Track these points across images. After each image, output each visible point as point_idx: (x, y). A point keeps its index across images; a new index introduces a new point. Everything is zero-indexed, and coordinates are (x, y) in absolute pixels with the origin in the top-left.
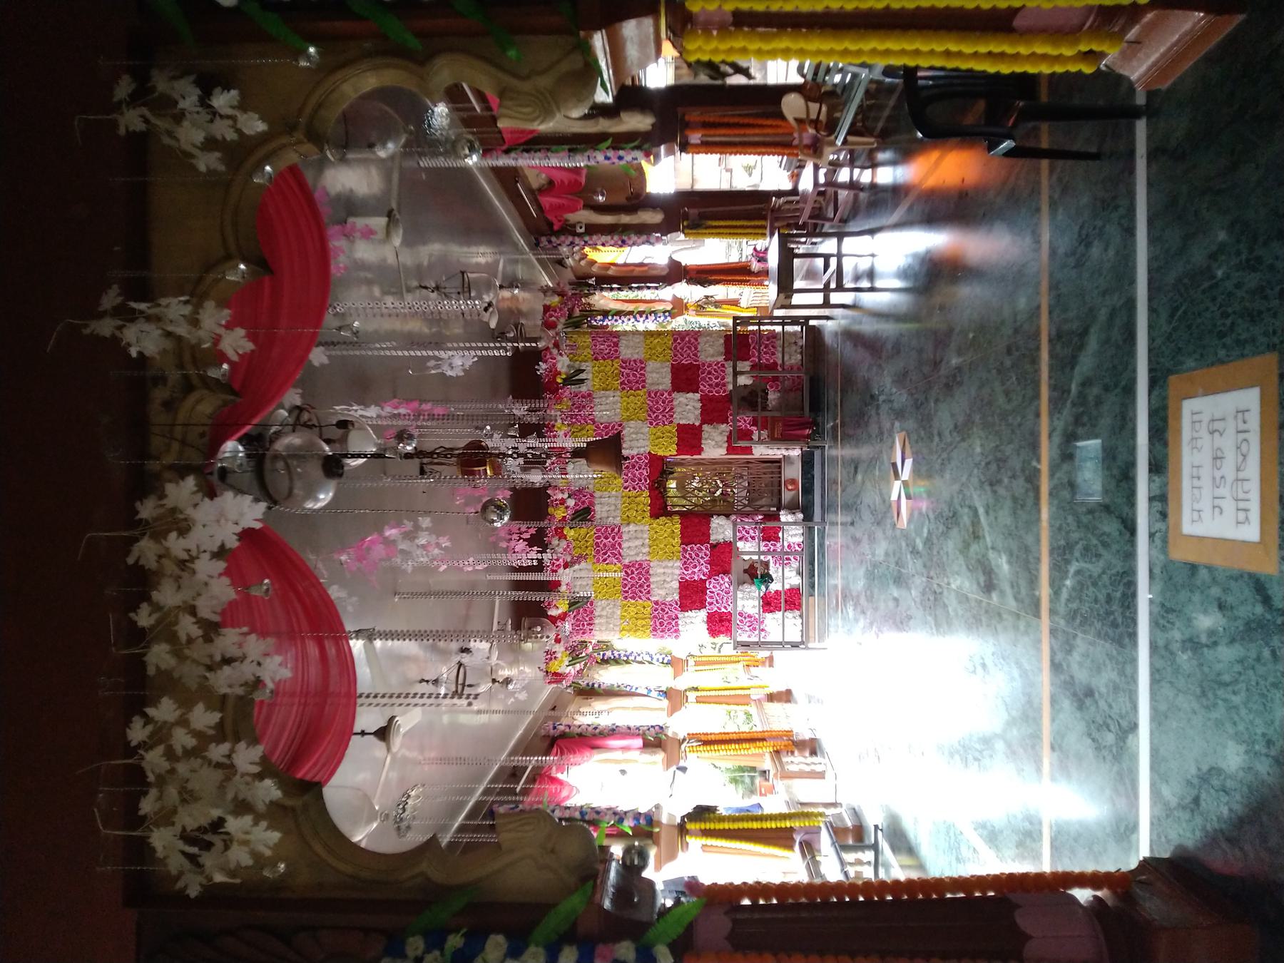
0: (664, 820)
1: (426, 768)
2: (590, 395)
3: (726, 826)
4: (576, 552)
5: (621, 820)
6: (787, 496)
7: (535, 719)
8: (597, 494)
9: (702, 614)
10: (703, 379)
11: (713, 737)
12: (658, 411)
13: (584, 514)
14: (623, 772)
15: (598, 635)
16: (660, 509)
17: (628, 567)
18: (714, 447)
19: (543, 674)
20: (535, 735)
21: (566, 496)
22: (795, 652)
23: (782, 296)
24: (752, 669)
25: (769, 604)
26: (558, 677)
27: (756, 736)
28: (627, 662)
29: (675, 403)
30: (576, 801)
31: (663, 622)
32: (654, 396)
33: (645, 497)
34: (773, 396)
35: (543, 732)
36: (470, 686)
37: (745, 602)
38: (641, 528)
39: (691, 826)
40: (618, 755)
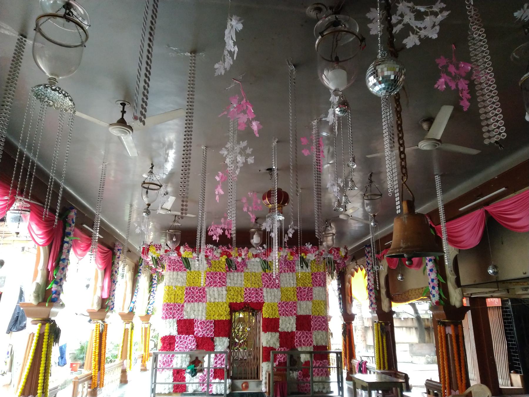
0: (53, 310)
1: (101, 167)
2: (294, 271)
3: (44, 349)
4: (212, 262)
5: (56, 283)
6: (239, 383)
7: (124, 240)
8: (243, 274)
9: (174, 333)
10: (303, 334)
11: (104, 339)
12: (286, 307)
13: (231, 265)
14: (88, 286)
15: (167, 273)
16: (234, 308)
17: (204, 290)
18: (267, 339)
19: (149, 244)
20: (116, 240)
21: (243, 257)
22: (149, 391)
23: (367, 385)
24: (141, 359)
25: (178, 374)
26: (146, 251)
27: (102, 365)
28: (150, 291)
29: (290, 317)
30: (72, 255)
31: (172, 309)
32: (294, 305)
33: (240, 300)
34: (295, 375)
35: (117, 243)
36: (147, 192)
37: (180, 358)
38: (224, 298)
39: (47, 326)
40: (99, 284)
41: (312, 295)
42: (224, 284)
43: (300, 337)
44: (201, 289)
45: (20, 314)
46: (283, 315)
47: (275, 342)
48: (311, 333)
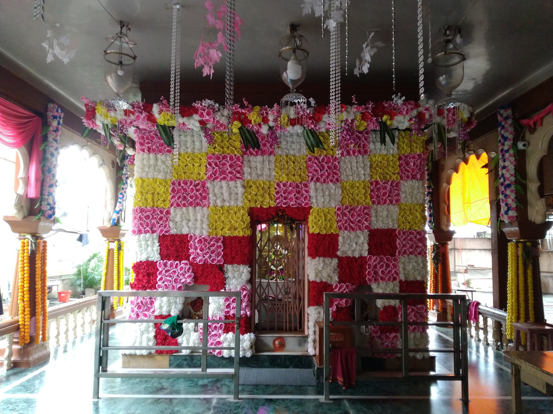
2: (366, 152)
42: (238, 175)
44: (198, 184)
47: (332, 274)
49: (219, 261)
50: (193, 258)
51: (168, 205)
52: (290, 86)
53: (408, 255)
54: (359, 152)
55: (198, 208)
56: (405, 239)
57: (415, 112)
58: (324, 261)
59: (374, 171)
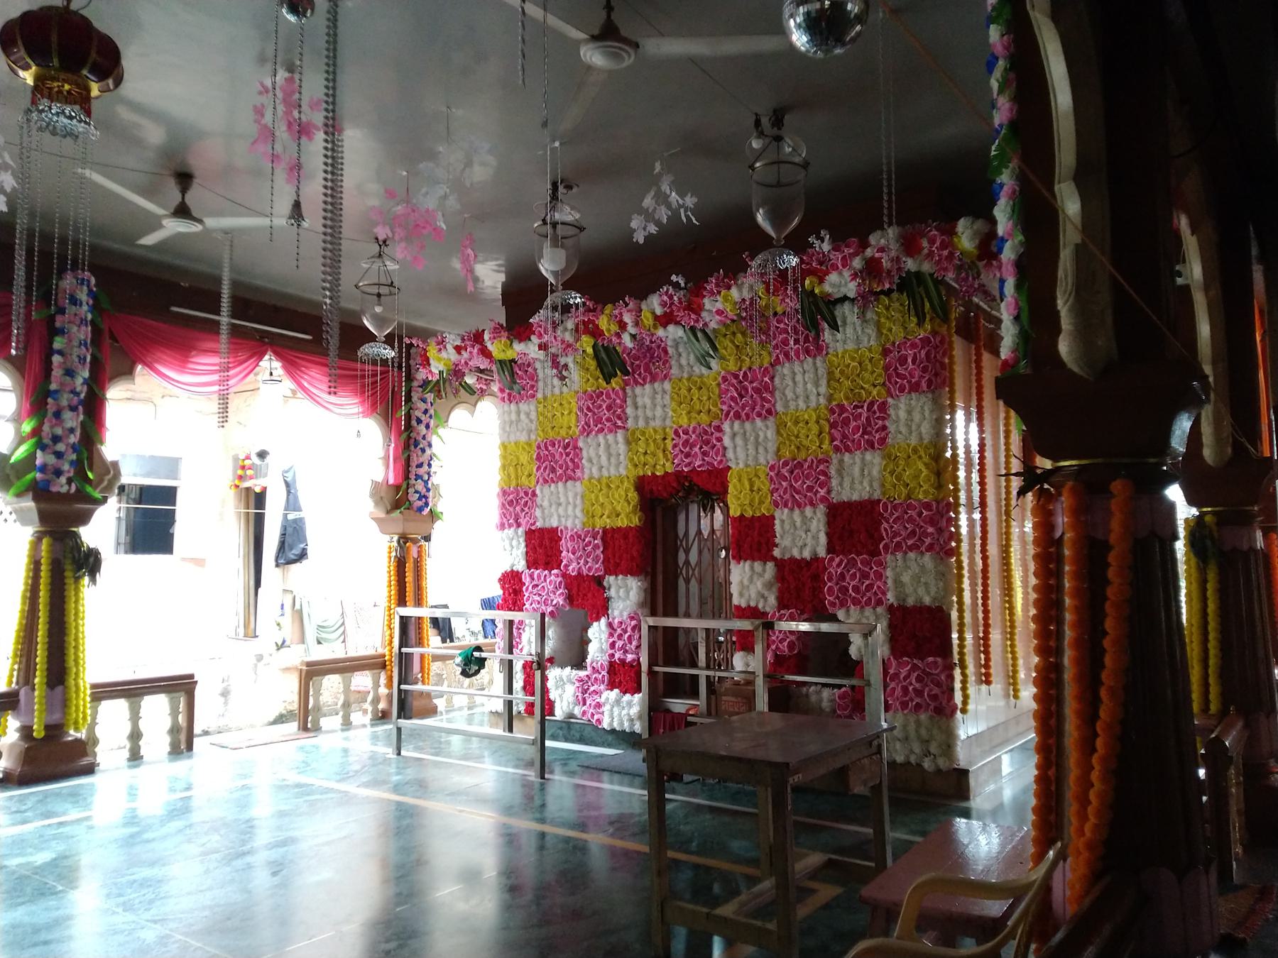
2: (819, 349)
12: (797, 477)
18: (748, 582)
33: (664, 466)
41: (884, 428)
42: (619, 423)
43: (842, 577)
44: (568, 444)
45: (290, 530)
46: (786, 505)
47: (766, 594)
48: (880, 564)
49: (597, 570)
50: (566, 566)
51: (533, 483)
52: (551, 280)
53: (906, 553)
54: (807, 352)
55: (570, 483)
56: (898, 518)
57: (857, 263)
58: (752, 568)
59: (836, 385)
